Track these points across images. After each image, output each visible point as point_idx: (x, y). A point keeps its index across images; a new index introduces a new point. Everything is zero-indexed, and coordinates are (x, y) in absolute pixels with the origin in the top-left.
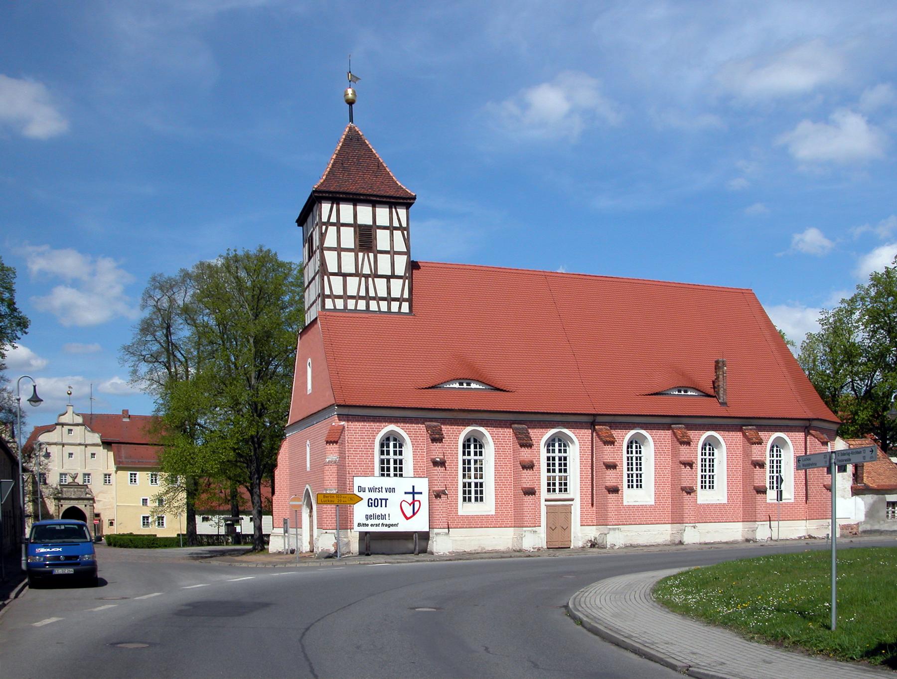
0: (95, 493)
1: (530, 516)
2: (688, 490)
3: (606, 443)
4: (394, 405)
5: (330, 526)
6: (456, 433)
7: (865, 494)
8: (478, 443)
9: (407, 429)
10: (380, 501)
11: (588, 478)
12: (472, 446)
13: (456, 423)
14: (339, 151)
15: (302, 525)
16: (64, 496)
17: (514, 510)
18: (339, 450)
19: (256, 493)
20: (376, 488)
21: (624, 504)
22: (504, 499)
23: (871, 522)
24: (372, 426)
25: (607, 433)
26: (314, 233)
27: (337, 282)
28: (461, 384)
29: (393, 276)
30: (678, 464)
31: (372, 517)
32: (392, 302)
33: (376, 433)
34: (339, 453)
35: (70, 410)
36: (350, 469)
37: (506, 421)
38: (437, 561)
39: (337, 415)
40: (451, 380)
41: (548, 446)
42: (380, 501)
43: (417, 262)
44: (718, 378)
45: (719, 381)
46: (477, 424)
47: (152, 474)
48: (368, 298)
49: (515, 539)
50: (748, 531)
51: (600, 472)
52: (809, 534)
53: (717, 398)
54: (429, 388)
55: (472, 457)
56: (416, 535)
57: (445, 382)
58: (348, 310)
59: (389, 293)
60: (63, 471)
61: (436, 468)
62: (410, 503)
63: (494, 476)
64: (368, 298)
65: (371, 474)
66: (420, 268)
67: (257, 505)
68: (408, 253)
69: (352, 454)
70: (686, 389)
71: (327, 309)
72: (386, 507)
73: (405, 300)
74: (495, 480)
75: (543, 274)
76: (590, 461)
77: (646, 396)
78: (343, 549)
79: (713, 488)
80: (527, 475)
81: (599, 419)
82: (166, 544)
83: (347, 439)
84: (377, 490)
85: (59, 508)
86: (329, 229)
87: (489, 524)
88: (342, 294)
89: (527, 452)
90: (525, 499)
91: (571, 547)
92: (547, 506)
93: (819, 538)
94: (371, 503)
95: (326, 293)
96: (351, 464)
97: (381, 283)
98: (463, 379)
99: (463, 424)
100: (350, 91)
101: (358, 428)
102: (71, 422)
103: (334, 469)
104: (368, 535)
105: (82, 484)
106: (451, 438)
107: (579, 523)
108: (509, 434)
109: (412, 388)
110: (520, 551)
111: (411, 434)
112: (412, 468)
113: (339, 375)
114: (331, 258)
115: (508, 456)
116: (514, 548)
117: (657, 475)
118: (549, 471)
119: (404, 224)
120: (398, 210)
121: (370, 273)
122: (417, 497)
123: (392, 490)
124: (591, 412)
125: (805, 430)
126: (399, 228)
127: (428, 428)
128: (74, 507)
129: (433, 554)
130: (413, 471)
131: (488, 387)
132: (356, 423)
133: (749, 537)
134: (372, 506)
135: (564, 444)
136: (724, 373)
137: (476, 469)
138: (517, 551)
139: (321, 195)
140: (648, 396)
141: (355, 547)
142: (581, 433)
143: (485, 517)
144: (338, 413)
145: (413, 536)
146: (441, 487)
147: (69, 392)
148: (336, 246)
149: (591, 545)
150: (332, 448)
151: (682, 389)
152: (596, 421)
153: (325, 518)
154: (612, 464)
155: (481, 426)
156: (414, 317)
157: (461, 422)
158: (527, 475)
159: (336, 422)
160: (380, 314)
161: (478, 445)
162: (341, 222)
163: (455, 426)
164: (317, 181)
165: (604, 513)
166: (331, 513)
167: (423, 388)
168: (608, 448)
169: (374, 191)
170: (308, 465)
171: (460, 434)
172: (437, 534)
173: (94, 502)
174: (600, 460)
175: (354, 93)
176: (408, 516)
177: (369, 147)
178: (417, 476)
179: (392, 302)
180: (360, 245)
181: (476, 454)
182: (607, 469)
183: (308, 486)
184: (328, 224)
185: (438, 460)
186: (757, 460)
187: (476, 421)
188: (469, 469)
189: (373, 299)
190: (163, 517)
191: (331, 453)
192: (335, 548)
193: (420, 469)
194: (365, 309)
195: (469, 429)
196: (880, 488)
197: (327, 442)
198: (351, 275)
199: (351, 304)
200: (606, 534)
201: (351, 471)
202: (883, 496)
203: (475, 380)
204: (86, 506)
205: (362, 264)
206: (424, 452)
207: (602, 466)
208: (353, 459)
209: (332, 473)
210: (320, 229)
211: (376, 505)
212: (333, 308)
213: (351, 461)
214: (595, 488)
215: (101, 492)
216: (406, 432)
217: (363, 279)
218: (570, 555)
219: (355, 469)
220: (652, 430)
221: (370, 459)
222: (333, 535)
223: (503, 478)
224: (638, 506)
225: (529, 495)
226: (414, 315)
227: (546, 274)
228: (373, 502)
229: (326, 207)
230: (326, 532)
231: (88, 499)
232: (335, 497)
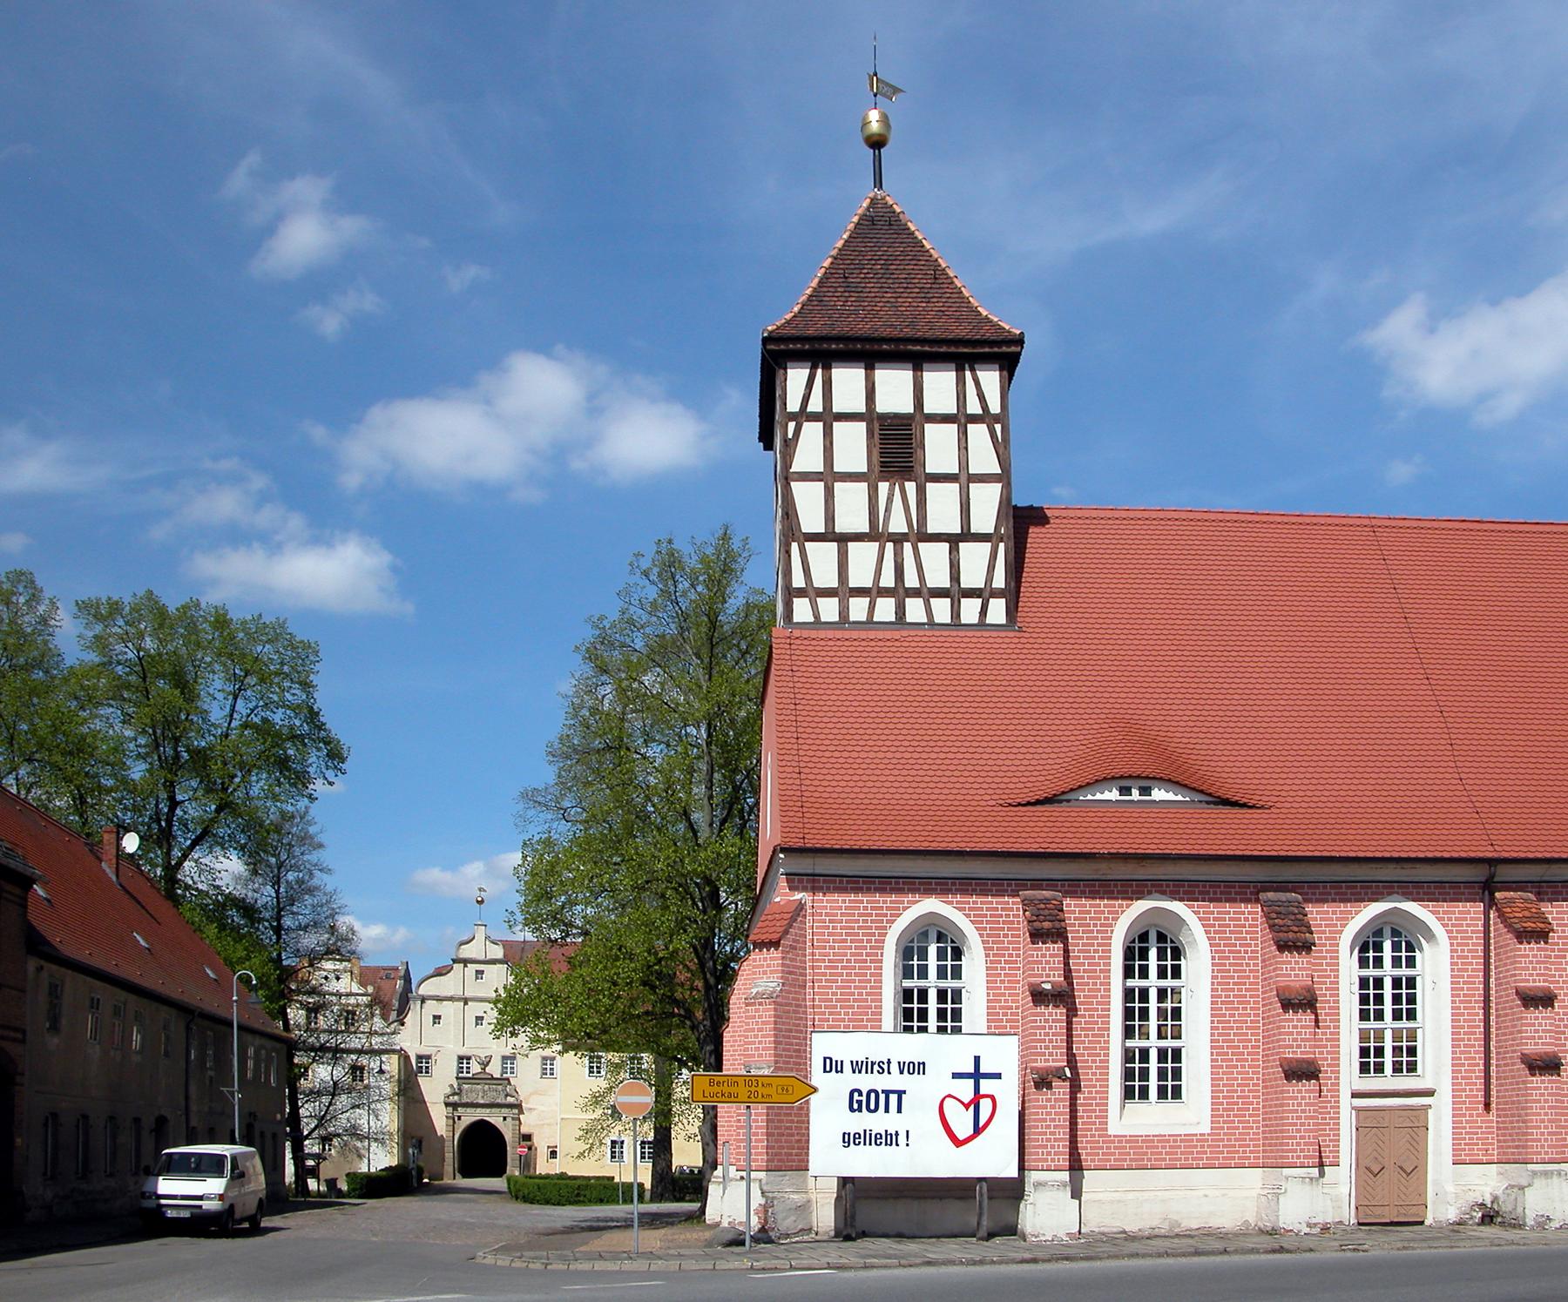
0: (523, 1095)
3: (1523, 936)
4: (934, 846)
10: (882, 1097)
11: (1475, 1033)
12: (1153, 953)
13: (1105, 892)
14: (840, 250)
16: (465, 1100)
17: (1264, 1120)
18: (783, 965)
20: (873, 1064)
24: (878, 902)
25: (1528, 909)
27: (823, 558)
28: (1125, 791)
29: (967, 535)
31: (862, 1140)
32: (963, 601)
33: (888, 922)
34: (783, 971)
35: (480, 934)
37: (1244, 884)
38: (993, 1262)
39: (786, 874)
40: (1097, 781)
41: (1364, 948)
42: (882, 1097)
43: (1042, 508)
46: (1163, 893)
47: (590, 1057)
48: (901, 591)
49: (1263, 1199)
51: (1507, 1015)
54: (1038, 802)
58: (850, 623)
60: (464, 1051)
61: (1042, 1009)
62: (966, 1102)
63: (1209, 1031)
64: (901, 591)
66: (1048, 523)
68: (1004, 478)
72: (899, 1111)
73: (996, 594)
74: (1212, 1041)
75: (1366, 522)
78: (786, 1223)
81: (1504, 873)
82: (603, 1197)
83: (809, 937)
84: (876, 1067)
85: (454, 1122)
90: (1288, 1092)
91: (1427, 1222)
92: (1358, 1110)
94: (860, 1102)
96: (820, 1000)
97: (935, 557)
98: (1130, 777)
99: (1127, 892)
100: (874, 116)
101: (841, 908)
102: (482, 957)
104: (849, 1186)
105: (499, 1076)
106: (1092, 931)
107: (1448, 1157)
108: (1253, 919)
110: (1273, 1232)
111: (982, 922)
113: (803, 776)
115: (1249, 977)
116: (1260, 1224)
117: (1217, 1028)
118: (1364, 1015)
119: (995, 407)
120: (978, 372)
122: (986, 1086)
123: (918, 1068)
124: (1481, 855)
126: (985, 417)
127: (1026, 903)
128: (482, 1120)
130: (985, 1018)
131: (1197, 797)
132: (836, 897)
134: (860, 1110)
137: (1162, 1013)
139: (782, 347)
141: (825, 1216)
143: (1127, 1142)
144: (789, 871)
146: (1053, 1061)
147: (479, 899)
149: (1483, 1216)
150: (765, 959)
152: (1495, 880)
154: (1540, 994)
156: (1018, 634)
162: (834, 411)
163: (1102, 898)
164: (781, 313)
165: (1519, 1128)
167: (1019, 804)
168: (1530, 949)
169: (919, 330)
170: (138, 937)
171: (1116, 919)
172: (1039, 1185)
173: (521, 1112)
174: (1508, 983)
175: (885, 119)
176: (961, 1137)
177: (916, 238)
178: (997, 1031)
179: (963, 601)
180: (883, 464)
181: (1162, 974)
182: (1526, 1006)
184: (803, 415)
185: (1048, 986)
188: (1144, 1014)
189: (915, 593)
190: (622, 1142)
191: (765, 973)
195: (1141, 906)
198: (858, 537)
199: (858, 609)
200: (1522, 1188)
203: (1161, 779)
204: (505, 1119)
207: (1513, 1001)
208: (823, 987)
211: (872, 1106)
212: (812, 620)
213: (819, 994)
214: (1493, 1062)
215: (535, 1093)
216: (968, 916)
217: (890, 546)
218: (1404, 1248)
219: (830, 1014)
226: (1020, 630)
227: (1374, 522)
228: (864, 1098)
231: (511, 1106)
232: (741, 1083)
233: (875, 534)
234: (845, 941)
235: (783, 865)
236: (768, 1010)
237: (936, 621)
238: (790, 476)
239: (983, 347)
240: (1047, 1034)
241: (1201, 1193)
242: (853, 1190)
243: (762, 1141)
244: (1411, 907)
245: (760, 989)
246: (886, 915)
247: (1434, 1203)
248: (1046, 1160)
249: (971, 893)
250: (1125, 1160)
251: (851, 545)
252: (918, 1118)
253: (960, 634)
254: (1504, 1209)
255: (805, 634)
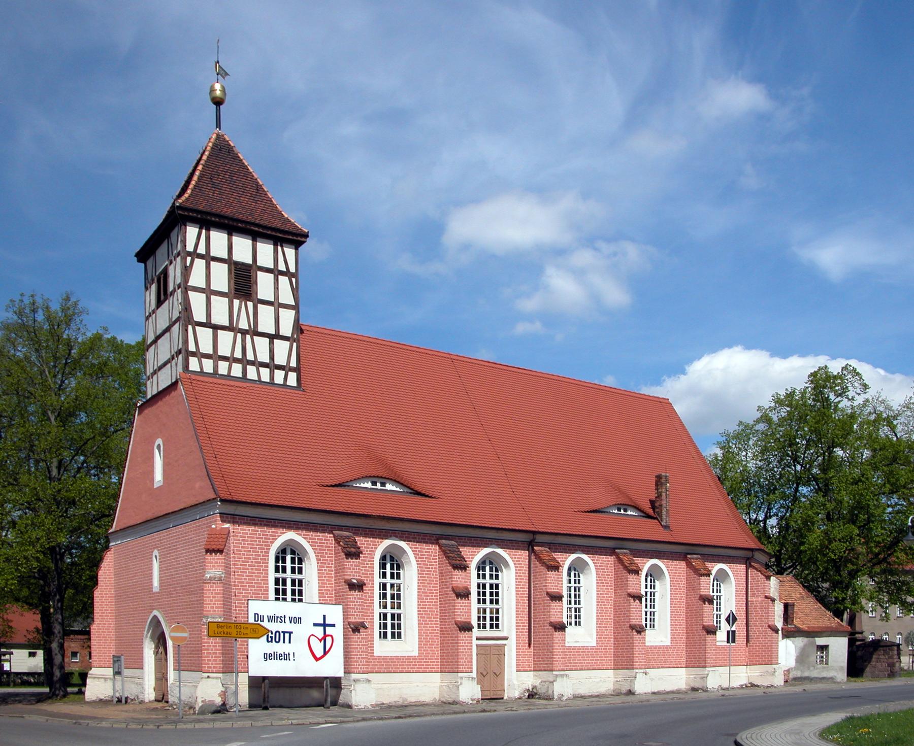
1: (466, 658)
2: (639, 629)
5: (214, 667)
6: (372, 548)
7: (795, 637)
8: (395, 562)
9: (310, 539)
10: (282, 635)
11: (524, 611)
13: (371, 535)
14: (206, 161)
15: (143, 665)
19: (57, 620)
20: (277, 617)
21: (646, 645)
22: (429, 636)
23: (802, 668)
24: (266, 531)
25: (549, 556)
26: (171, 269)
27: (205, 334)
28: (374, 483)
30: (625, 598)
31: (273, 657)
32: (275, 370)
36: (236, 589)
37: (431, 535)
39: (220, 513)
42: (282, 635)
44: (659, 496)
45: (662, 500)
46: (397, 537)
48: (245, 361)
50: (695, 678)
52: (750, 682)
53: (658, 520)
54: (336, 486)
55: (488, 581)
56: (327, 682)
57: (355, 479)
58: (218, 374)
59: (272, 357)
61: (352, 592)
63: (417, 606)
64: (245, 361)
65: (264, 597)
66: (303, 333)
67: (58, 635)
69: (240, 569)
70: (625, 507)
71: (191, 371)
72: (290, 642)
73: (292, 370)
75: (448, 356)
76: (527, 590)
77: (585, 513)
78: (231, 701)
79: (580, 625)
80: (461, 606)
81: (539, 538)
84: (279, 619)
86: (195, 262)
87: (411, 668)
88: (211, 352)
89: (461, 575)
93: (764, 687)
94: (272, 637)
95: (190, 350)
96: (238, 582)
97: (262, 344)
99: (380, 535)
100: (218, 87)
103: (218, 588)
104: (267, 681)
109: (315, 484)
110: (455, 703)
111: (315, 546)
112: (317, 592)
114: (197, 301)
116: (442, 699)
117: (420, 605)
119: (292, 270)
120: (285, 249)
121: (247, 328)
122: (329, 630)
123: (297, 620)
125: (746, 562)
126: (287, 273)
129: (351, 708)
130: (318, 595)
131: (406, 490)
132: (245, 527)
133: (696, 685)
134: (272, 641)
135: (496, 568)
136: (667, 491)
138: (449, 703)
139: (186, 213)
140: (587, 514)
141: (244, 697)
142: (517, 555)
143: (383, 659)
144: (221, 512)
145: (323, 683)
146: (359, 619)
148: (205, 287)
150: (214, 559)
151: (622, 507)
152: (536, 541)
153: (206, 657)
155: (402, 540)
156: (303, 393)
157: (400, 535)
158: (461, 606)
159: (218, 525)
160: (261, 384)
161: (395, 565)
166: (216, 650)
167: (327, 486)
171: (376, 548)
175: (223, 90)
176: (318, 656)
177: (243, 163)
180: (236, 290)
183: (155, 613)
184: (195, 255)
185: (355, 581)
186: (705, 595)
187: (396, 533)
189: (252, 363)
191: (214, 566)
192: (222, 698)
193: (327, 594)
194: (241, 376)
195: (387, 542)
196: (811, 630)
197: (208, 551)
198: (223, 328)
201: (238, 593)
202: (813, 639)
205: (239, 315)
206: (332, 571)
209: (216, 593)
210: (184, 261)
211: (277, 640)
212: (199, 370)
213: (238, 579)
216: (309, 542)
217: (239, 335)
220: (594, 554)
221: (263, 577)
222: (220, 681)
223: (428, 608)
224: (580, 648)
225: (465, 631)
226: (304, 390)
228: (273, 635)
229: (192, 232)
230: (208, 677)
232: (233, 625)
233: (231, 328)
234: (250, 551)
235: (218, 508)
236: (219, 587)
237: (205, 371)
238: (188, 288)
239: (288, 235)
240: (355, 605)
241: (415, 685)
242: (256, 683)
243: (220, 657)
244: (500, 551)
245: (212, 575)
246: (269, 539)
247: (507, 689)
248: (358, 668)
249: (310, 530)
250: (382, 668)
251: (219, 331)
252: (298, 646)
253: (273, 388)
254: (540, 692)
255: (193, 377)
